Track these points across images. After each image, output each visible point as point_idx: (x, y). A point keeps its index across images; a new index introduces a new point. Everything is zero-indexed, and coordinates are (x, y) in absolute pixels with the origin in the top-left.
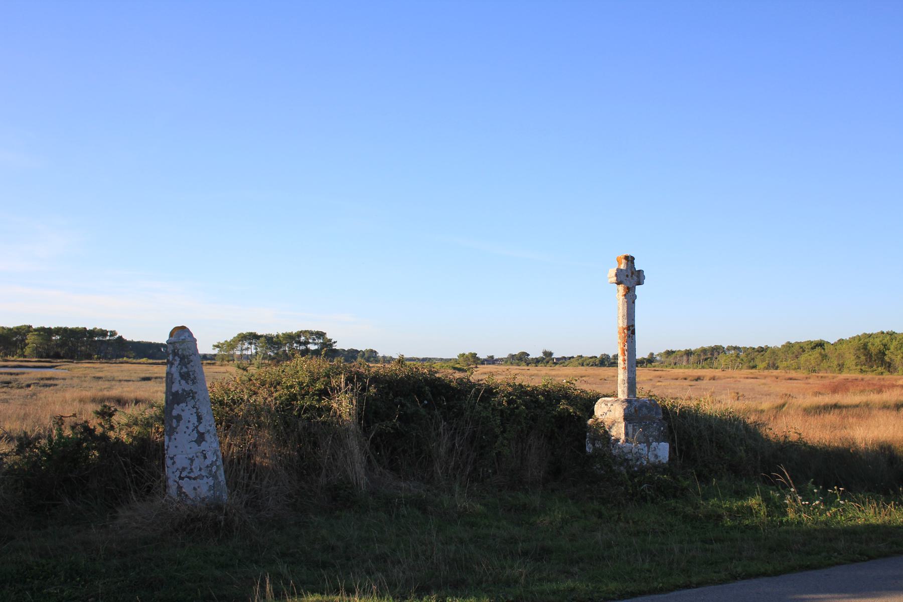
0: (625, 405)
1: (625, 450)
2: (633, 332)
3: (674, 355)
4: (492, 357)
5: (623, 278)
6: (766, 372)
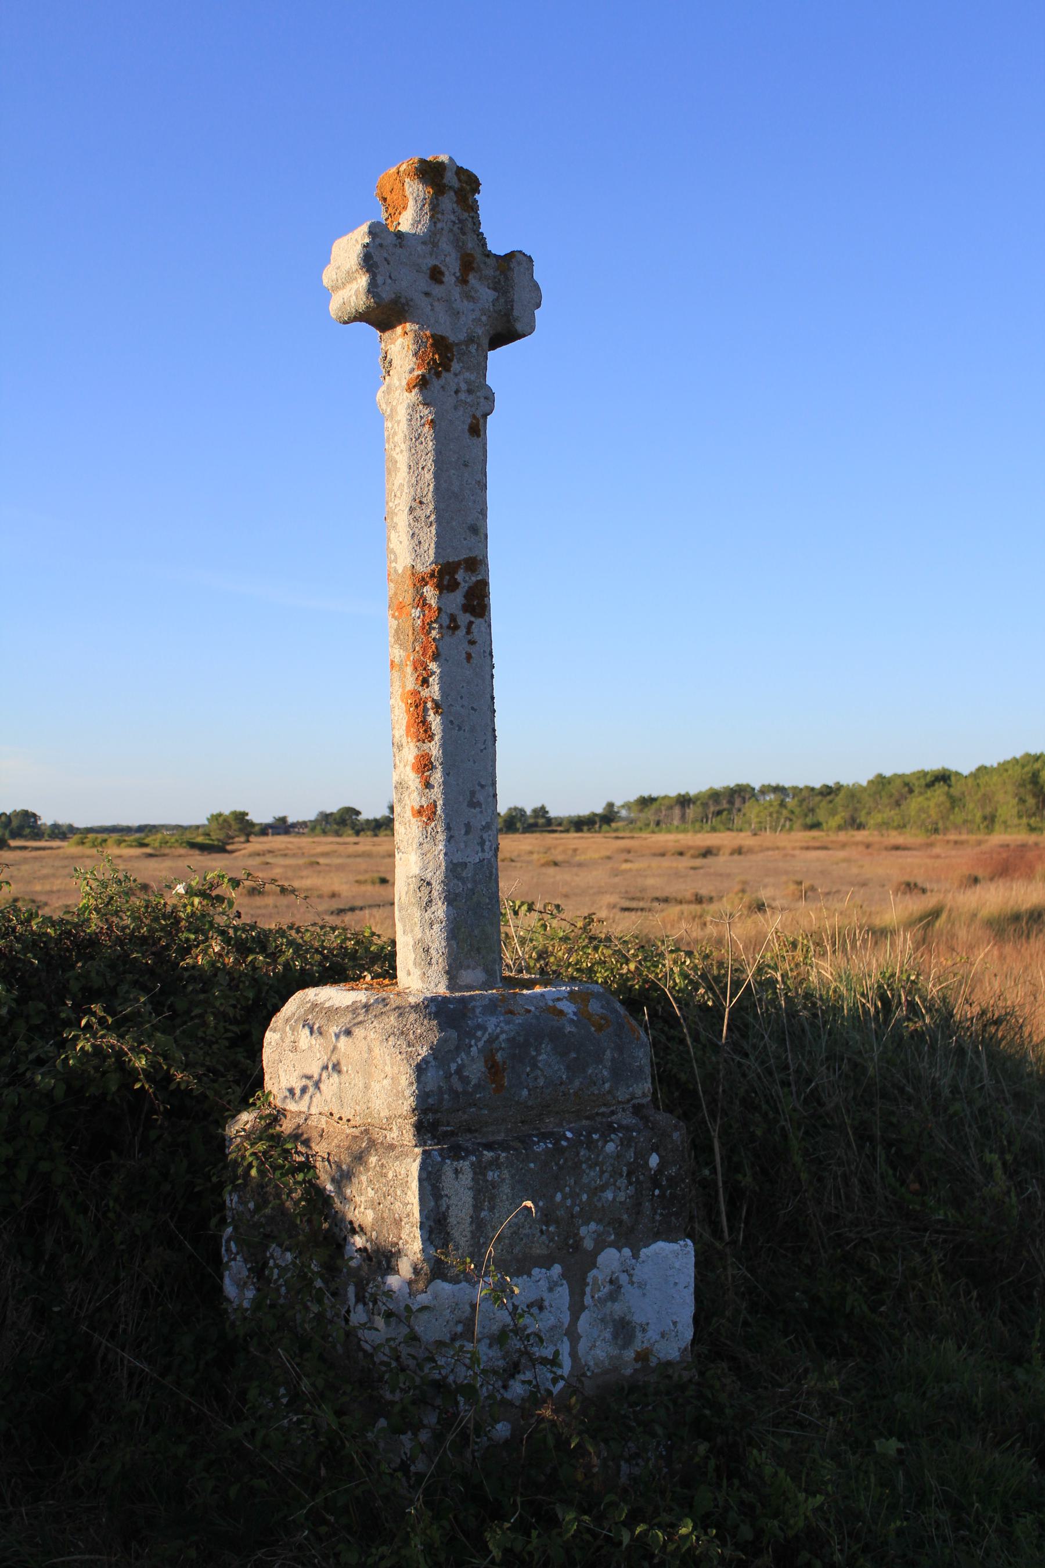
0: (426, 1037)
1: (431, 1330)
2: (477, 602)
3: (655, 806)
4: (283, 820)
5: (410, 283)
6: (842, 836)
